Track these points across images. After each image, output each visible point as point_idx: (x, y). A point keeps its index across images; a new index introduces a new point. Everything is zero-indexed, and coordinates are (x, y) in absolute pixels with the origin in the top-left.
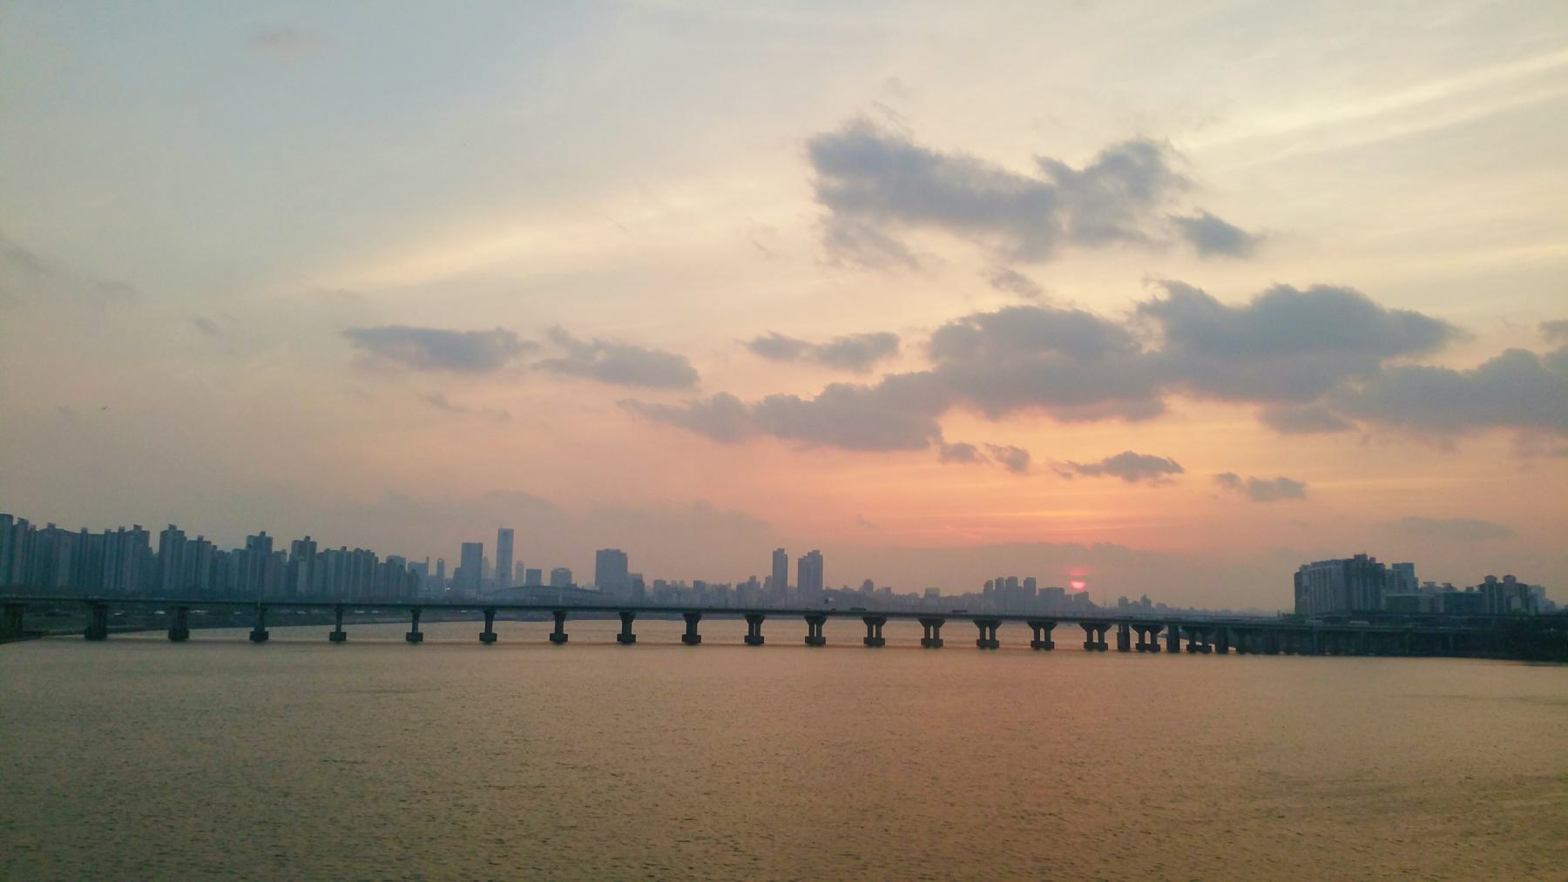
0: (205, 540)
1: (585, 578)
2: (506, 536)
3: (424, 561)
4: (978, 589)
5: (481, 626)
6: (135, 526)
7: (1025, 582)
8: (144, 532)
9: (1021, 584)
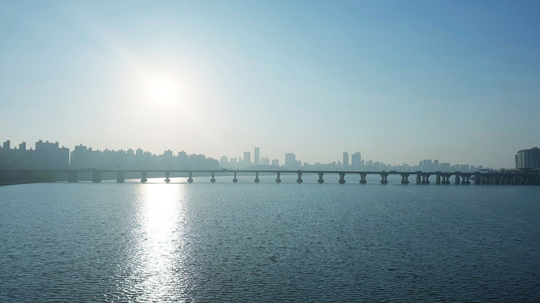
0: (123, 150)
1: (282, 163)
2: (257, 150)
3: (235, 158)
4: (418, 164)
5: (255, 177)
6: (129, 149)
7: (434, 161)
8: (141, 150)
9: (433, 162)
